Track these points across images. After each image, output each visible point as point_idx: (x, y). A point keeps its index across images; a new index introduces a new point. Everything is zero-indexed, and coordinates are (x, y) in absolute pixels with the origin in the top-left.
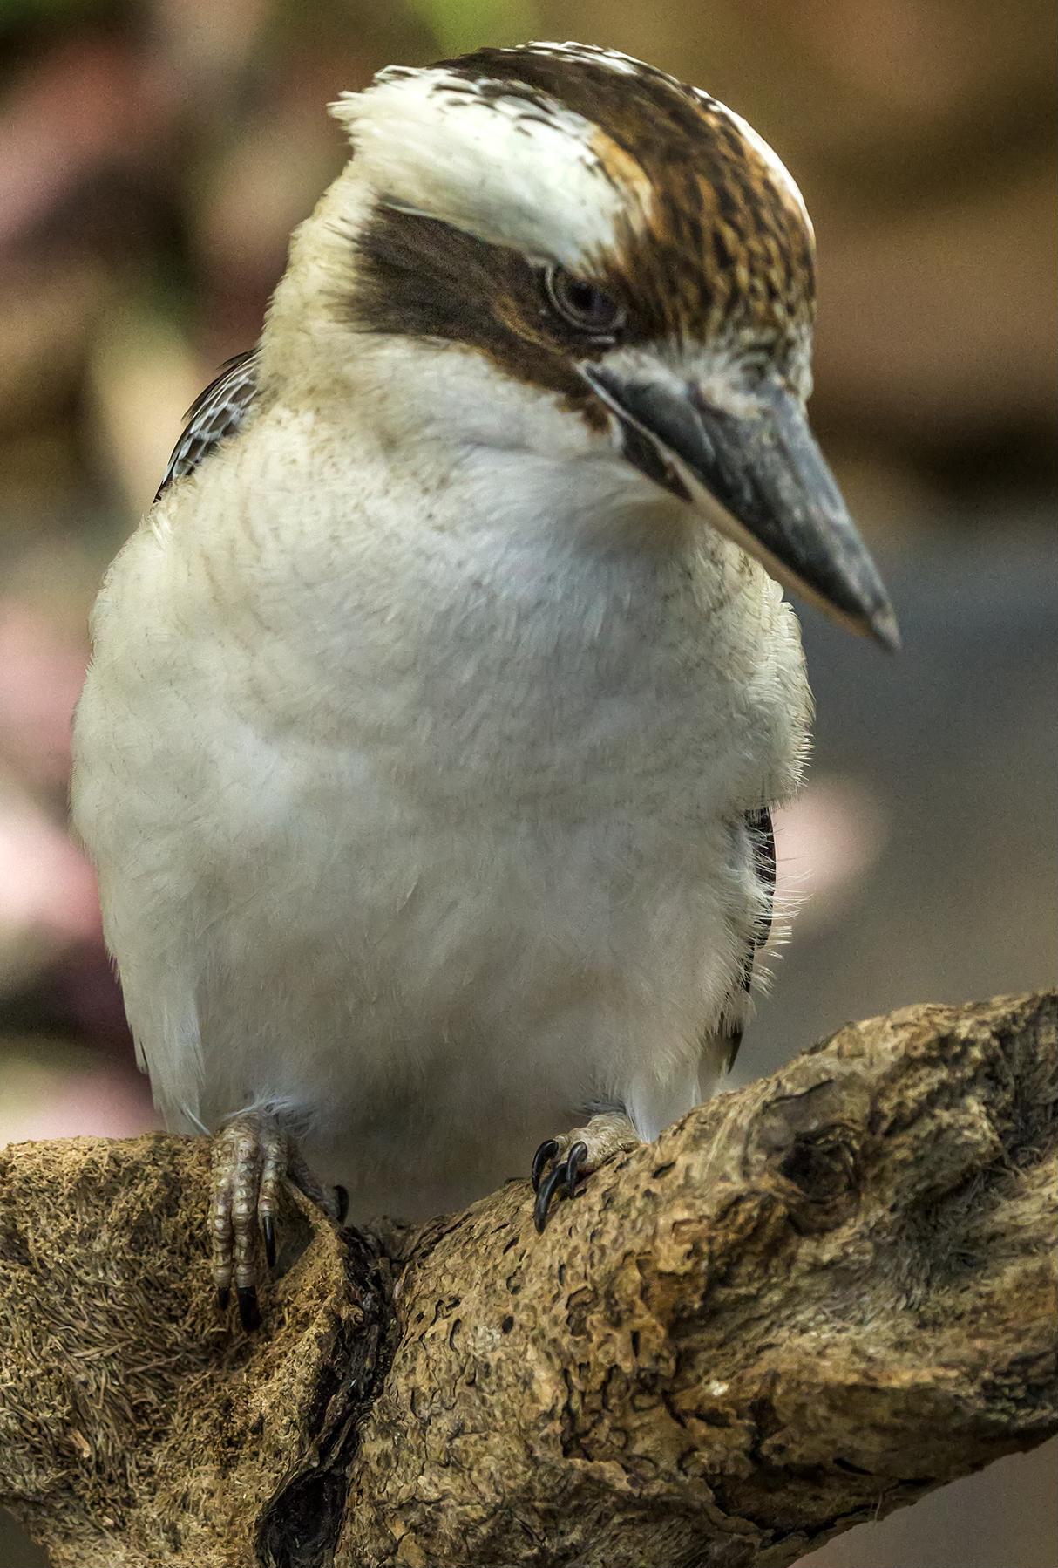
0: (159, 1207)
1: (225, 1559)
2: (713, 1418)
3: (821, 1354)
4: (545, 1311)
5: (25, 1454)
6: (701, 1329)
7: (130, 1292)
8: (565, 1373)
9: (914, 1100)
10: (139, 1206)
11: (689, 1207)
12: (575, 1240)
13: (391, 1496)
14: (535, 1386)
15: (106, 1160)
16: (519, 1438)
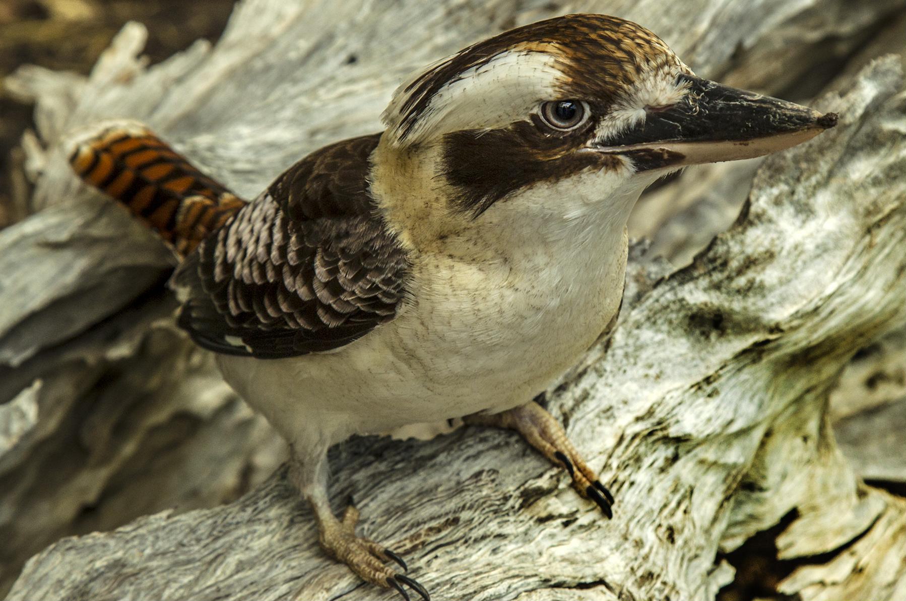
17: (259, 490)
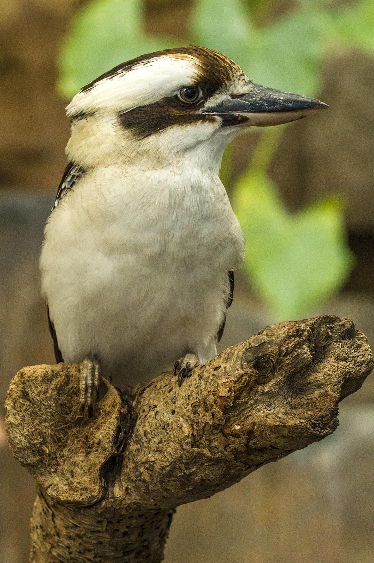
0: (64, 384)
1: (89, 479)
2: (236, 435)
3: (266, 417)
4: (185, 408)
5: (31, 452)
6: (230, 412)
7: (57, 407)
8: (192, 425)
9: (291, 347)
10: (59, 383)
11: (227, 378)
12: (192, 389)
13: (140, 460)
14: (183, 429)
15: (50, 371)
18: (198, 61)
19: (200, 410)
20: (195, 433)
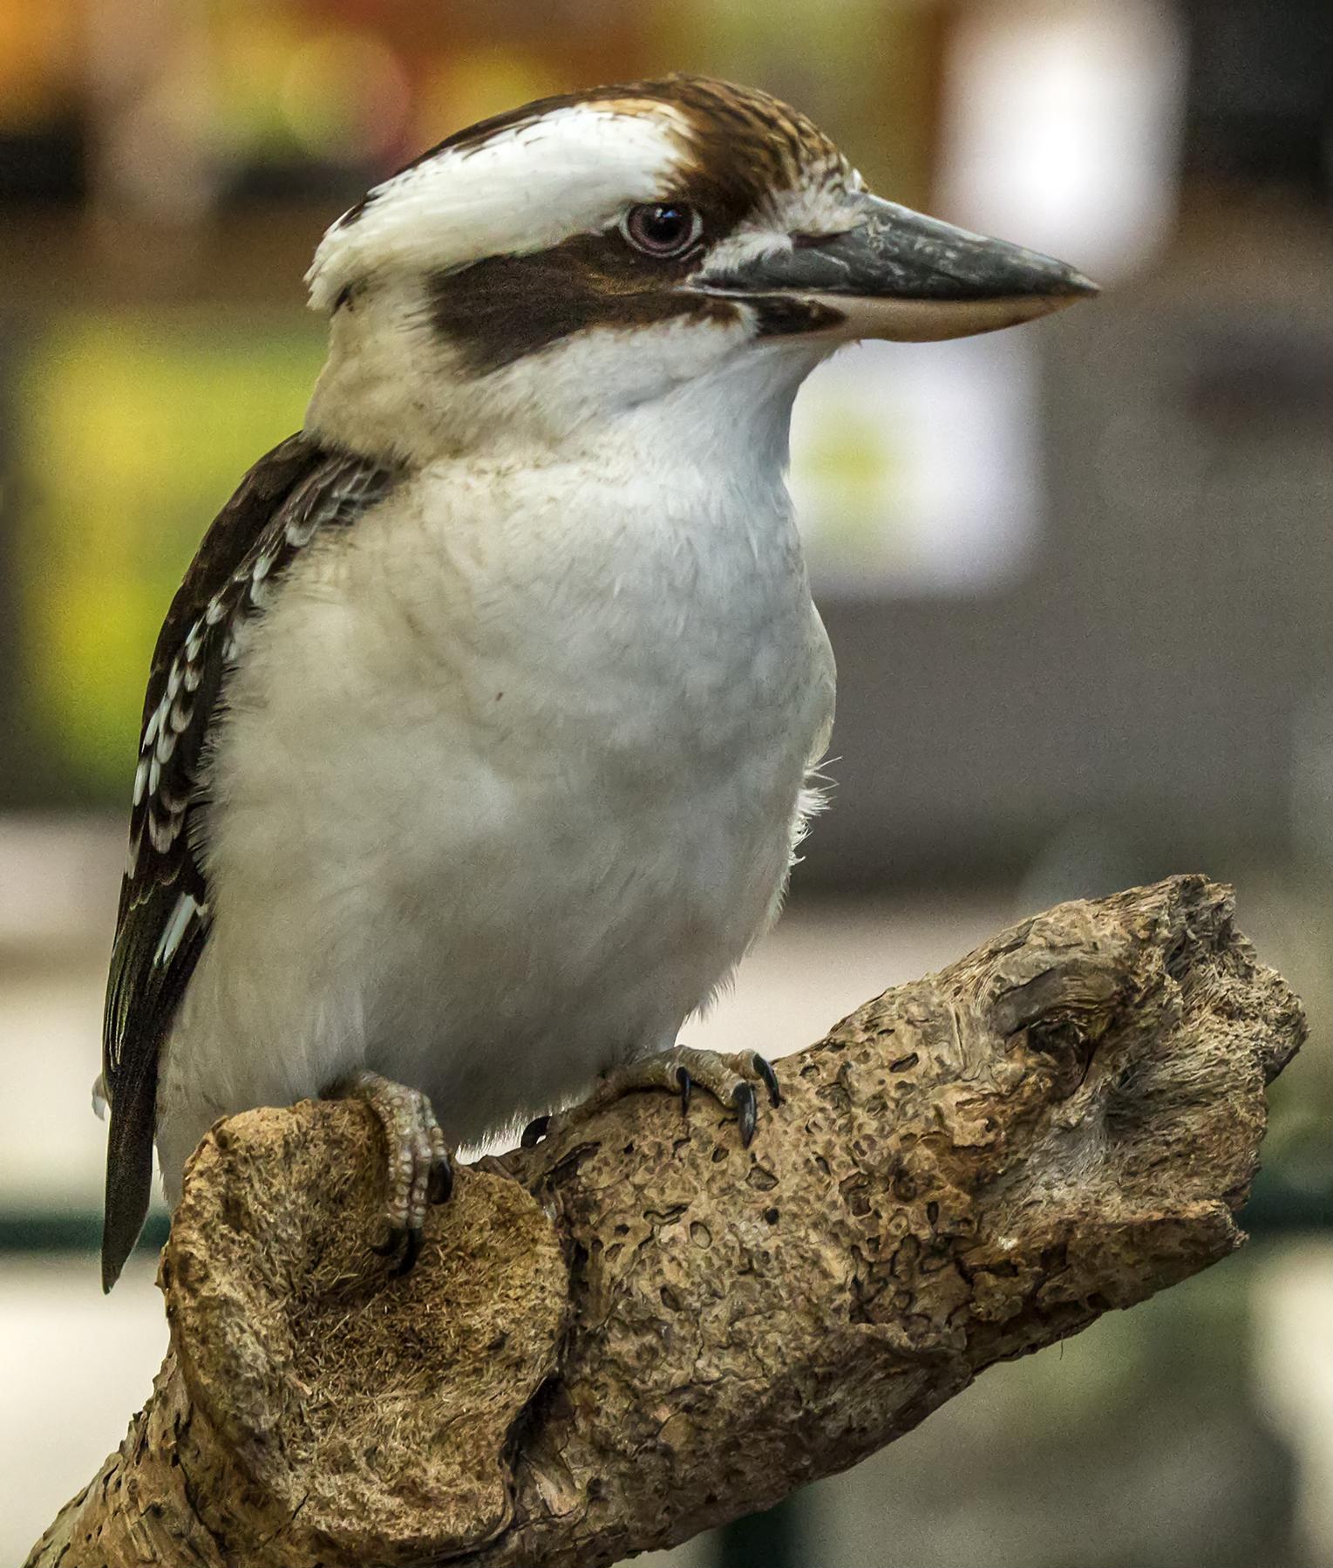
8: (854, 1249)
16: (808, 1313)
17: (610, 1287)
18: (681, 123)
19: (878, 1196)
20: (862, 1276)
